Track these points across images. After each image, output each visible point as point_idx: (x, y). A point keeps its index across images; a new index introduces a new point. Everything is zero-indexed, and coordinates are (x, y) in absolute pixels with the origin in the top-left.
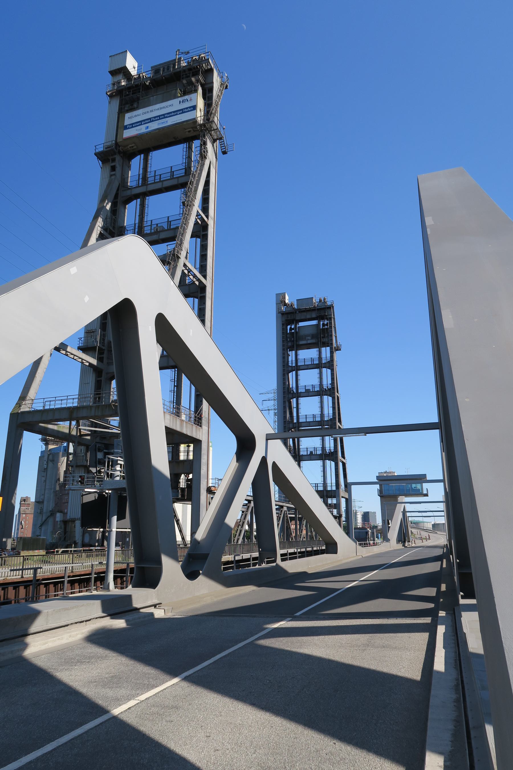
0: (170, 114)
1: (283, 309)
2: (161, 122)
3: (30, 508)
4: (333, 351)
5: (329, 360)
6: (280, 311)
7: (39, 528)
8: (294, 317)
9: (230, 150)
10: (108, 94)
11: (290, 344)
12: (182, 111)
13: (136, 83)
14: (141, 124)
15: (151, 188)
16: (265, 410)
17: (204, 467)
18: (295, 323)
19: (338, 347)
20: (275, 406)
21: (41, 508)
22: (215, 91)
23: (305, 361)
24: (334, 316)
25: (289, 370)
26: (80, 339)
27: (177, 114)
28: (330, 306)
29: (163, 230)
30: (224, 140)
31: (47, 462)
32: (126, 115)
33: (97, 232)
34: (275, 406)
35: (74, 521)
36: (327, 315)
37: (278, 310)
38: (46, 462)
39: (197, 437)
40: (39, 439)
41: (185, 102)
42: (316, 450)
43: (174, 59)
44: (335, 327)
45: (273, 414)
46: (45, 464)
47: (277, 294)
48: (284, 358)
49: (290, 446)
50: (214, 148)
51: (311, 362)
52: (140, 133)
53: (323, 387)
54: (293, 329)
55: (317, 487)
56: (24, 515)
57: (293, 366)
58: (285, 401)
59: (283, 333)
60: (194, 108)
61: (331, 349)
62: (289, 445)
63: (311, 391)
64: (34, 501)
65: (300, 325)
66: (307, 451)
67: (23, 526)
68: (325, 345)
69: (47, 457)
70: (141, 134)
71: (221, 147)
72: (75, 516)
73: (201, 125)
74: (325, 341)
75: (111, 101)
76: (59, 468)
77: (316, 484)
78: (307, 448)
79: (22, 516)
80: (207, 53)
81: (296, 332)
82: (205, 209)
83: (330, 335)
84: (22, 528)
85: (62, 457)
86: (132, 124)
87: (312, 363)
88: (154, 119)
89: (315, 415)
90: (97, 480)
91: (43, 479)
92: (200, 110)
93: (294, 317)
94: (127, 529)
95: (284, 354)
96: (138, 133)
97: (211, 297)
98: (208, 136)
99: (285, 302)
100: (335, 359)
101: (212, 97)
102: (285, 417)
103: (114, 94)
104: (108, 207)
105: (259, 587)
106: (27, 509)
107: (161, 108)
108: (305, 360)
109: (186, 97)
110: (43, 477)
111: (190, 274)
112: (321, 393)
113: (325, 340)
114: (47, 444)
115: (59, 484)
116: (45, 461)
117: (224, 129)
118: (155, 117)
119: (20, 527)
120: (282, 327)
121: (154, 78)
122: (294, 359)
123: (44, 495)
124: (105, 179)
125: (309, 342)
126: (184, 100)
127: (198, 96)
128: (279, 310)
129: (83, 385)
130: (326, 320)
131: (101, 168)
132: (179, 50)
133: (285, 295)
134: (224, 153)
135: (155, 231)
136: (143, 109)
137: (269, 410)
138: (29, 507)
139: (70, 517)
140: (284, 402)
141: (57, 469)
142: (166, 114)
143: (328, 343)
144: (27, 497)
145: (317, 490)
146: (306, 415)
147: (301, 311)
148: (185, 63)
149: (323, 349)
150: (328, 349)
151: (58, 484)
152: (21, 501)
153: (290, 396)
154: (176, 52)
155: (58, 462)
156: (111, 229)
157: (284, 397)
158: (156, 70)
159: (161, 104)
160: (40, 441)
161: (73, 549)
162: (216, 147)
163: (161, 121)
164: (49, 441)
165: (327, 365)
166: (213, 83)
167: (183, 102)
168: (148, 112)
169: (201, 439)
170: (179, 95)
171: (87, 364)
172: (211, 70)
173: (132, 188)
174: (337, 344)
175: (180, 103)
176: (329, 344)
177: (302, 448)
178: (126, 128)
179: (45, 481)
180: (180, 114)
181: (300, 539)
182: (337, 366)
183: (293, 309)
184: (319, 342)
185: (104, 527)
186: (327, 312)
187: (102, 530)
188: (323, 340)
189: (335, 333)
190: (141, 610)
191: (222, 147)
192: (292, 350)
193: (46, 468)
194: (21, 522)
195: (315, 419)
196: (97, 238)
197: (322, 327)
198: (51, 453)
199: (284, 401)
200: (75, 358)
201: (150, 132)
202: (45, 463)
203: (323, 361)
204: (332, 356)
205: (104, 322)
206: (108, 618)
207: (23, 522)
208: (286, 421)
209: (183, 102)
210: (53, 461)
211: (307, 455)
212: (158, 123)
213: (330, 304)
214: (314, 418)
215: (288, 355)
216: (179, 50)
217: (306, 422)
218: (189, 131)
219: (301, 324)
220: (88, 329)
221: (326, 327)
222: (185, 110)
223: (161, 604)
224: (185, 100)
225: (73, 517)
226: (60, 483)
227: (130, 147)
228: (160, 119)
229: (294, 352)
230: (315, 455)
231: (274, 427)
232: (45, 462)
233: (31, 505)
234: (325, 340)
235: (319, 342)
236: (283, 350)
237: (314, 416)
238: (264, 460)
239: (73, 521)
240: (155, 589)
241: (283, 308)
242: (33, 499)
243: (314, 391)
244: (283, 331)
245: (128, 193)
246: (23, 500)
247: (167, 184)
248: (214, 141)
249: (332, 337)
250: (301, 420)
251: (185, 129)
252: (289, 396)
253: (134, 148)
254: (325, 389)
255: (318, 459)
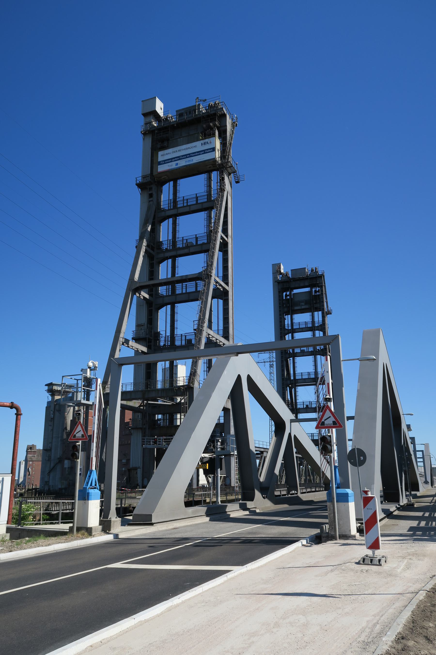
0: (195, 154)
1: (279, 278)
2: (188, 160)
3: (36, 456)
4: (324, 316)
5: (321, 324)
6: (276, 280)
7: (48, 474)
8: (289, 285)
9: (242, 180)
10: (143, 132)
11: (286, 310)
12: (204, 152)
13: (165, 126)
14: (172, 161)
15: (181, 211)
16: (261, 362)
17: (232, 428)
18: (290, 290)
19: (329, 312)
20: (270, 358)
21: (49, 455)
22: (228, 133)
23: (299, 324)
24: (325, 284)
25: (286, 332)
26: (133, 332)
27: (200, 154)
28: (321, 275)
29: (192, 246)
30: (237, 173)
31: (54, 412)
32: (159, 152)
33: (143, 251)
34: (270, 358)
35: (137, 469)
36: (318, 284)
37: (275, 279)
38: (53, 412)
39: (227, 406)
40: (46, 390)
41: (206, 144)
42: (311, 404)
43: (195, 105)
44: (326, 294)
45: (269, 366)
46: (52, 414)
47: (273, 264)
48: (281, 322)
49: (288, 400)
50: (229, 180)
51: (182, 340)
52: (171, 169)
53: (316, 348)
54: (288, 296)
55: (313, 437)
56: (31, 463)
57: (289, 329)
58: (283, 360)
59: (279, 300)
60: (214, 149)
61: (323, 313)
62: (287, 399)
63: (306, 351)
64: (42, 449)
65: (294, 293)
66: (303, 404)
67: (30, 473)
68: (317, 310)
69: (54, 407)
70: (172, 169)
71: (235, 178)
72: (135, 465)
73: (219, 165)
74: (317, 306)
75: (144, 138)
76: (66, 417)
77: (312, 434)
78: (303, 402)
79: (29, 463)
80: (221, 103)
81: (291, 299)
82: (225, 231)
83: (322, 301)
84: (29, 475)
85: (68, 408)
86: (165, 161)
87: (309, 377)
88: (182, 158)
89: (310, 373)
90: (164, 441)
91: (50, 428)
92: (218, 150)
93: (289, 285)
94: (223, 475)
95: (280, 318)
96: (169, 168)
97: (232, 299)
98: (225, 172)
99: (280, 271)
100: (327, 323)
101: (226, 137)
102: (283, 375)
103: (147, 132)
104: (149, 229)
105: (290, 505)
106: (33, 456)
107: (187, 149)
108: (299, 324)
109: (207, 140)
110: (50, 426)
111: (217, 284)
112: (315, 353)
113: (318, 305)
114: (53, 395)
115: (67, 433)
116: (52, 410)
117: (237, 164)
118: (183, 156)
119: (28, 473)
120: (279, 294)
121: (180, 122)
122: (290, 323)
123: (52, 443)
124: (144, 203)
125: (303, 307)
126: (205, 143)
127: (216, 139)
128: (275, 280)
129: (137, 366)
130: (317, 287)
131: (141, 194)
132: (198, 98)
133: (280, 266)
134: (237, 182)
135: (186, 246)
136: (172, 148)
137: (265, 362)
138: (35, 455)
139: (132, 466)
140: (282, 362)
141: (64, 418)
142: (191, 154)
143: (320, 308)
144: (33, 445)
145: (313, 439)
146: (302, 373)
147: (294, 280)
148: (203, 108)
149: (316, 313)
150: (320, 313)
151: (65, 433)
152: (27, 449)
153: (287, 356)
154: (196, 99)
155: (64, 412)
156: (152, 245)
157: (282, 357)
158: (180, 114)
159: (187, 145)
160: (46, 392)
161: (138, 489)
162: (230, 178)
163: (188, 159)
164: (55, 392)
165: (320, 328)
166: (226, 126)
167: (204, 145)
168: (176, 151)
169: (230, 408)
170: (201, 138)
171: (140, 352)
172: (224, 116)
173: (164, 210)
174: (328, 310)
175: (202, 145)
176: (321, 309)
177: (299, 402)
178: (160, 163)
179: (52, 430)
180: (202, 154)
181: (301, 482)
182: (328, 328)
183: (288, 278)
184: (312, 308)
185: (214, 474)
186: (319, 280)
187: (213, 475)
188: (316, 306)
189: (326, 299)
190: (251, 509)
191: (235, 176)
192: (288, 315)
193: (52, 417)
194: (28, 469)
195: (310, 376)
196: (143, 255)
197: (314, 293)
198: (57, 403)
199: (282, 361)
200: (133, 348)
201: (179, 168)
202: (52, 413)
203: (315, 324)
204: (324, 320)
205: (150, 317)
206: (242, 510)
207: (30, 469)
208: (284, 378)
209: (204, 145)
210: (59, 411)
211: (303, 408)
212: (185, 160)
213: (321, 273)
214: (309, 376)
215: (285, 319)
216: (198, 98)
217: (302, 379)
218: (210, 167)
219: (295, 291)
220: (138, 324)
221: (318, 293)
222: (206, 151)
223: (256, 507)
224: (206, 142)
225: (135, 466)
226: (67, 431)
227: (163, 178)
228: (187, 158)
229: (289, 316)
230: (310, 408)
231: (270, 378)
232: (52, 412)
233: (37, 452)
234: (318, 305)
235: (312, 308)
236: (280, 315)
237: (309, 374)
238: (290, 434)
239: (136, 469)
240: (253, 501)
241: (279, 277)
242: (40, 446)
243: (309, 352)
244: (279, 297)
245: (163, 214)
246: (29, 448)
247: (193, 208)
248: (229, 174)
249: (323, 303)
250: (297, 378)
251: (207, 166)
252: (286, 356)
253: (166, 178)
254: (318, 349)
255: (313, 412)
